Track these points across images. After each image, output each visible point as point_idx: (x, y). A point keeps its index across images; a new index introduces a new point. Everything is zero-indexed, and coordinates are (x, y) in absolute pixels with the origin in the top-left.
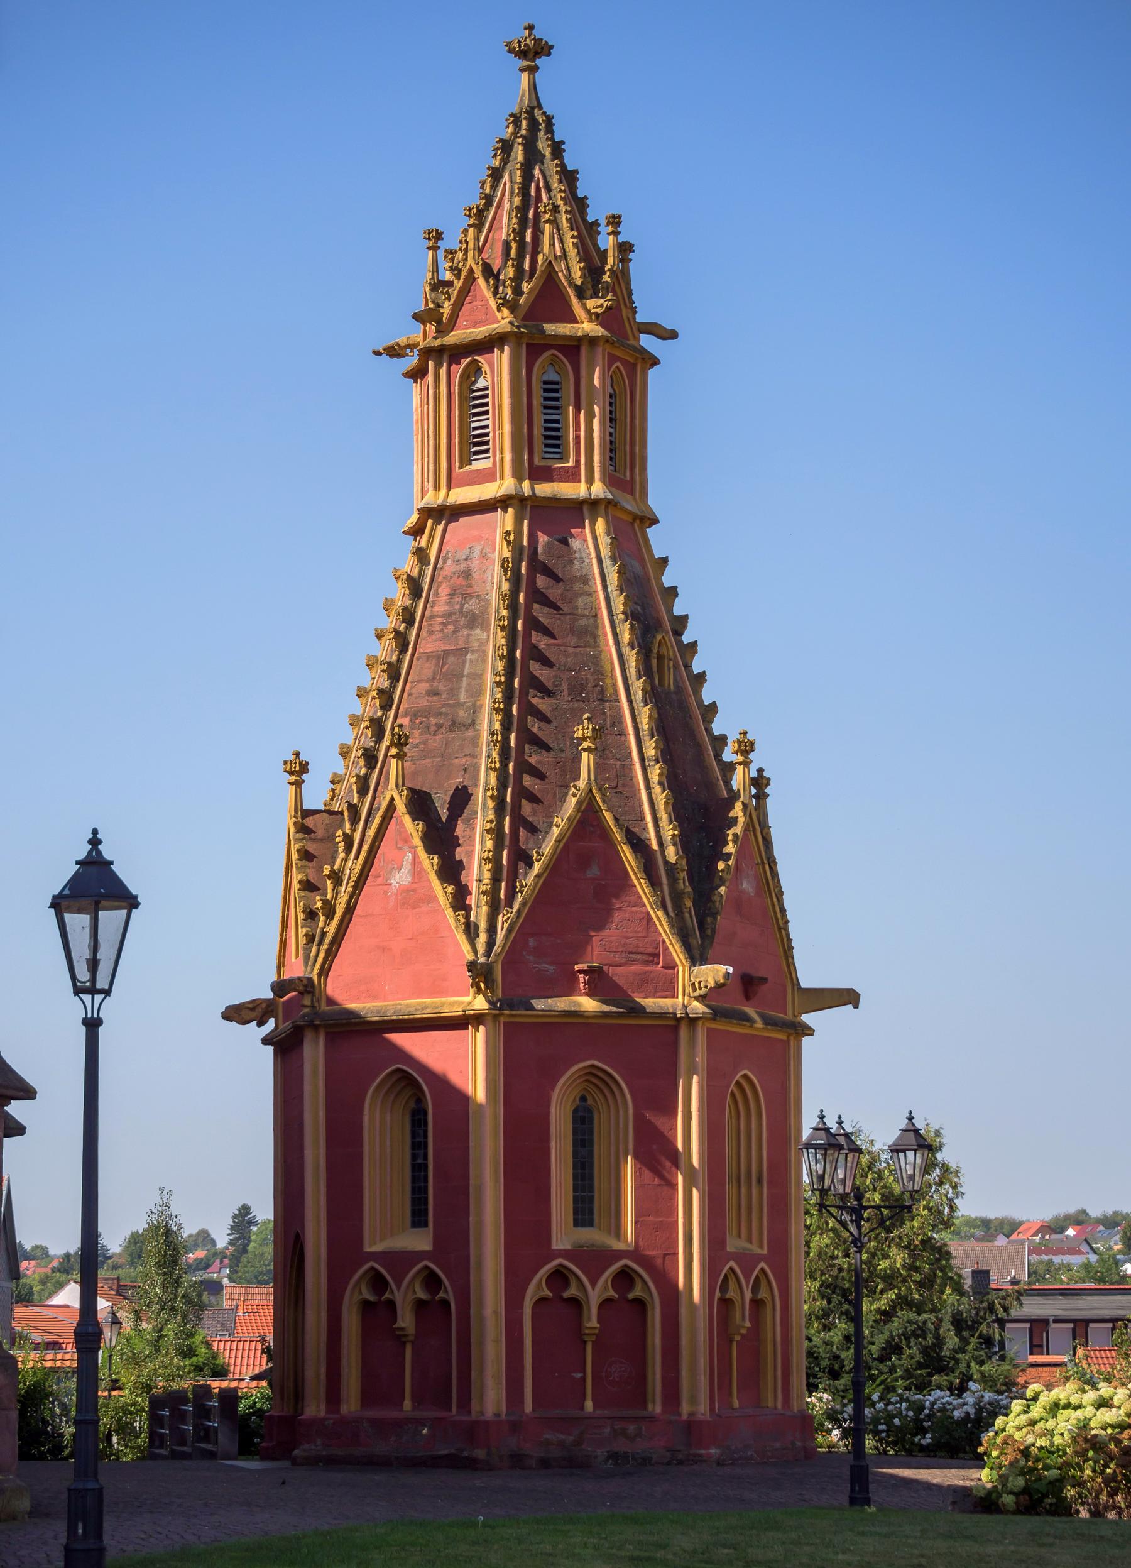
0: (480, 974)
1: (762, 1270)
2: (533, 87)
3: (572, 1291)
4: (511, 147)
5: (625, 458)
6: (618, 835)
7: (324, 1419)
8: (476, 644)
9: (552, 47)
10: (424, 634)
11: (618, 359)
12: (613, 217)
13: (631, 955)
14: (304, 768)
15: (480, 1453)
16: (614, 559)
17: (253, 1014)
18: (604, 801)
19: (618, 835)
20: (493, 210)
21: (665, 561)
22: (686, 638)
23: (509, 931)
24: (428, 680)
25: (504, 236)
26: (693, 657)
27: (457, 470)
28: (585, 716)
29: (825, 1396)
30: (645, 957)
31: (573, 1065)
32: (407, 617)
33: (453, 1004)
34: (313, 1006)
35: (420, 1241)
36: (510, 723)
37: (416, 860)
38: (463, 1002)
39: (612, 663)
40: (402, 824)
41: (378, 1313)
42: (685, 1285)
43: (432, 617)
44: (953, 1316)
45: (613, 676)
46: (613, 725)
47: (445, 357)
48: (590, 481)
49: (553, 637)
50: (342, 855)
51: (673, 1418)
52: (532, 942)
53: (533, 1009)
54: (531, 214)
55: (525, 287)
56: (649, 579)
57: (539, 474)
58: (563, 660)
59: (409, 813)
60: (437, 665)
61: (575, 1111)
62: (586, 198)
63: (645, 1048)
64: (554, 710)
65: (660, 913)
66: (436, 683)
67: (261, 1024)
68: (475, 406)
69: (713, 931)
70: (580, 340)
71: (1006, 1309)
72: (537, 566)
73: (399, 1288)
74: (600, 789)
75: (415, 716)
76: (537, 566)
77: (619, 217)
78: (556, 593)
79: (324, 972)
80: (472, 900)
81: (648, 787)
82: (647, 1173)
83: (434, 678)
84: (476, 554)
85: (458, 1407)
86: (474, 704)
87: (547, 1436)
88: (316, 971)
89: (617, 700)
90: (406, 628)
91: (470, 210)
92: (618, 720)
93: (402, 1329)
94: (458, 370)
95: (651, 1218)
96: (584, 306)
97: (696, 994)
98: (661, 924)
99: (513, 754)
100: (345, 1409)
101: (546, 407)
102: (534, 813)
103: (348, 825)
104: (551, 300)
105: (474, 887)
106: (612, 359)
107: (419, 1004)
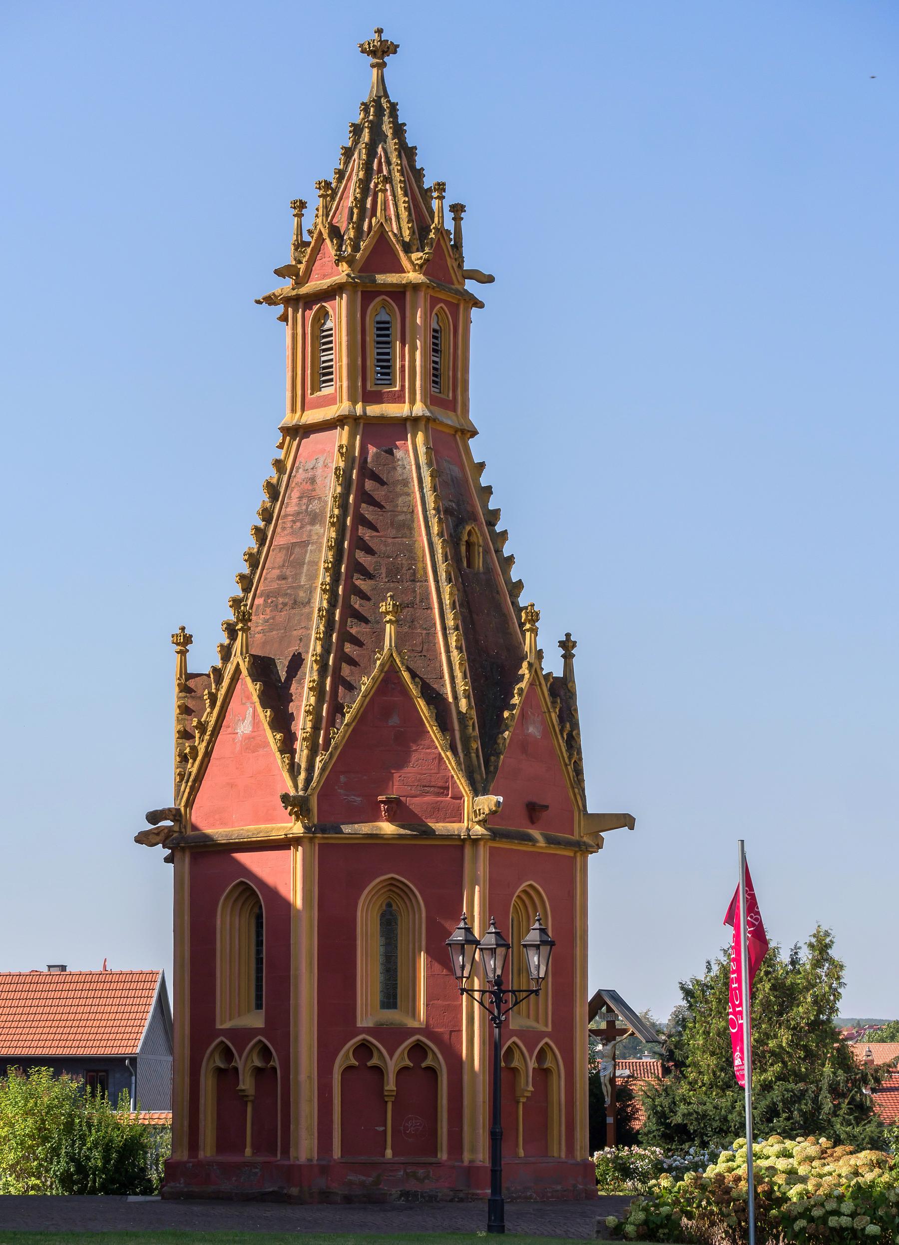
0: (298, 806)
2: (382, 80)
3: (374, 1061)
4: (362, 130)
5: (447, 380)
6: (414, 691)
7: (185, 1163)
8: (315, 537)
9: (398, 46)
10: (279, 530)
11: (441, 301)
12: (439, 184)
13: (425, 788)
14: (188, 640)
15: (294, 1191)
16: (429, 464)
17: (158, 839)
18: (403, 663)
19: (414, 691)
20: (344, 182)
21: (482, 465)
22: (498, 528)
23: (323, 769)
24: (279, 567)
25: (350, 204)
26: (504, 543)
27: (309, 396)
28: (389, 595)
29: (658, 1149)
30: (436, 790)
31: (375, 878)
32: (267, 516)
33: (279, 829)
34: (180, 832)
36: (336, 601)
38: (286, 827)
39: (424, 551)
40: (245, 684)
41: (227, 1076)
42: (467, 1056)
43: (286, 516)
44: (830, 1086)
45: (424, 561)
46: (421, 601)
47: (301, 304)
48: (413, 402)
49: (377, 531)
50: (208, 710)
51: (457, 1164)
52: (343, 778)
55: (363, 245)
56: (467, 481)
57: (371, 397)
59: (250, 675)
60: (286, 555)
61: (383, 915)
62: (422, 169)
63: (436, 864)
64: (373, 589)
68: (324, 344)
69: (496, 768)
70: (405, 286)
73: (240, 1057)
75: (268, 597)
76: (367, 473)
77: (444, 184)
78: (379, 494)
79: (189, 804)
80: (297, 745)
82: (437, 966)
83: (283, 566)
84: (320, 464)
86: (311, 587)
88: (183, 804)
89: (427, 581)
90: (266, 525)
91: (320, 183)
92: (426, 597)
93: (243, 1091)
94: (310, 314)
95: (440, 1002)
96: (410, 259)
97: (477, 819)
99: (337, 626)
100: (201, 1155)
101: (378, 343)
102: (352, 673)
103: (213, 686)
104: (382, 255)
105: (300, 735)
106: (434, 301)
107: (256, 829)
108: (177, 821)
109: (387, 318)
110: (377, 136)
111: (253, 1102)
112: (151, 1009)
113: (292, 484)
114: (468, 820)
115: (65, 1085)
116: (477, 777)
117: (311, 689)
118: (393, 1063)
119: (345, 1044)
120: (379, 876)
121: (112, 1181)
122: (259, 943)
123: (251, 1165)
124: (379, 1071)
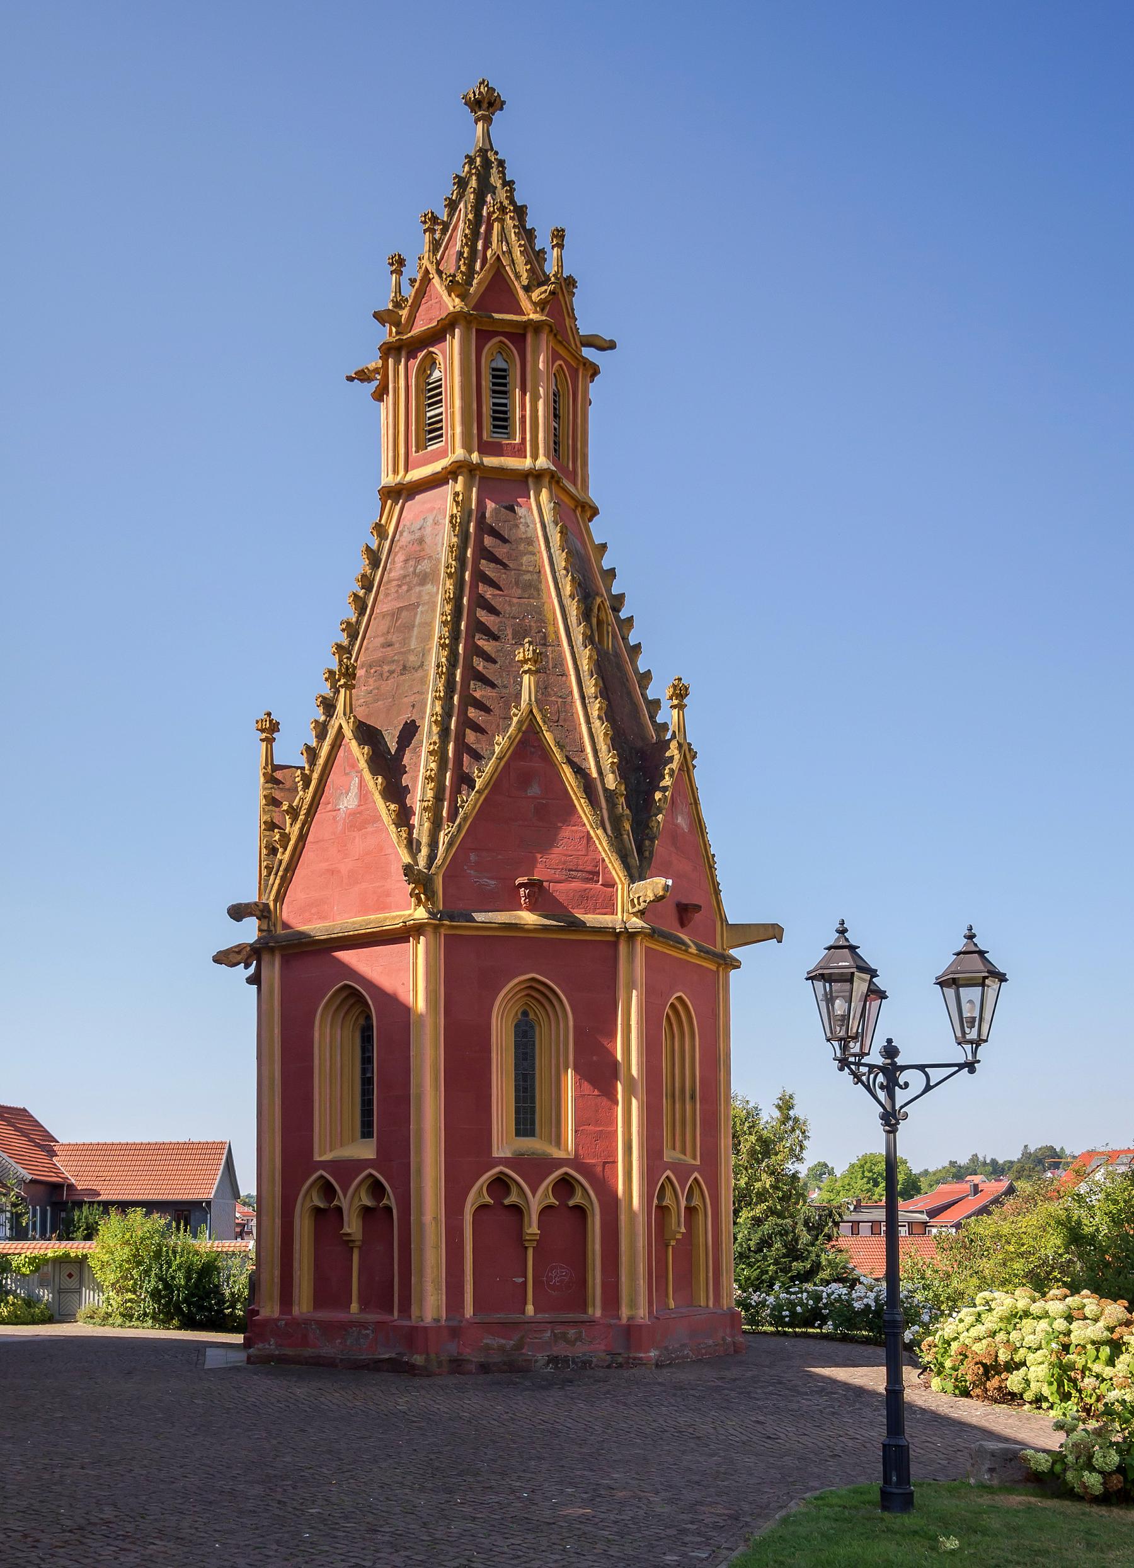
0: (421, 882)
1: (695, 1179)
2: (487, 135)
3: (513, 1198)
5: (568, 440)
6: (559, 756)
7: (278, 1320)
8: (426, 598)
9: (504, 103)
10: (381, 596)
14: (274, 727)
15: (418, 1359)
17: (239, 957)
21: (604, 546)
22: (623, 615)
23: (450, 844)
24: (383, 635)
26: (629, 630)
32: (367, 584)
35: (366, 1151)
36: (456, 661)
37: (362, 784)
39: (554, 613)
41: (327, 1218)
45: (555, 624)
46: (555, 667)
47: (404, 353)
48: (535, 457)
52: (473, 857)
53: (474, 921)
54: (482, 230)
57: (486, 448)
58: (508, 608)
63: (584, 961)
65: (600, 832)
66: (390, 636)
67: (247, 967)
69: (651, 853)
71: (840, 1215)
72: (484, 528)
73: (345, 1196)
74: (540, 710)
75: (371, 667)
76: (484, 528)
77: (563, 230)
78: (501, 551)
79: (280, 897)
80: (415, 820)
81: (588, 722)
85: (400, 1311)
87: (488, 1341)
88: (272, 898)
92: (560, 662)
93: (349, 1235)
94: (414, 364)
95: (591, 1127)
96: (530, 298)
97: (635, 910)
98: (601, 843)
99: (458, 687)
100: (296, 1311)
102: (478, 741)
108: (265, 917)
109: (503, 365)
110: (484, 188)
111: (360, 1248)
112: (222, 1167)
113: (396, 549)
114: (623, 912)
115: (155, 1221)
116: (631, 861)
117: (431, 753)
118: (537, 1200)
119: (477, 1179)
120: (517, 976)
121: (192, 1295)
122: (367, 1060)
124: (517, 1211)
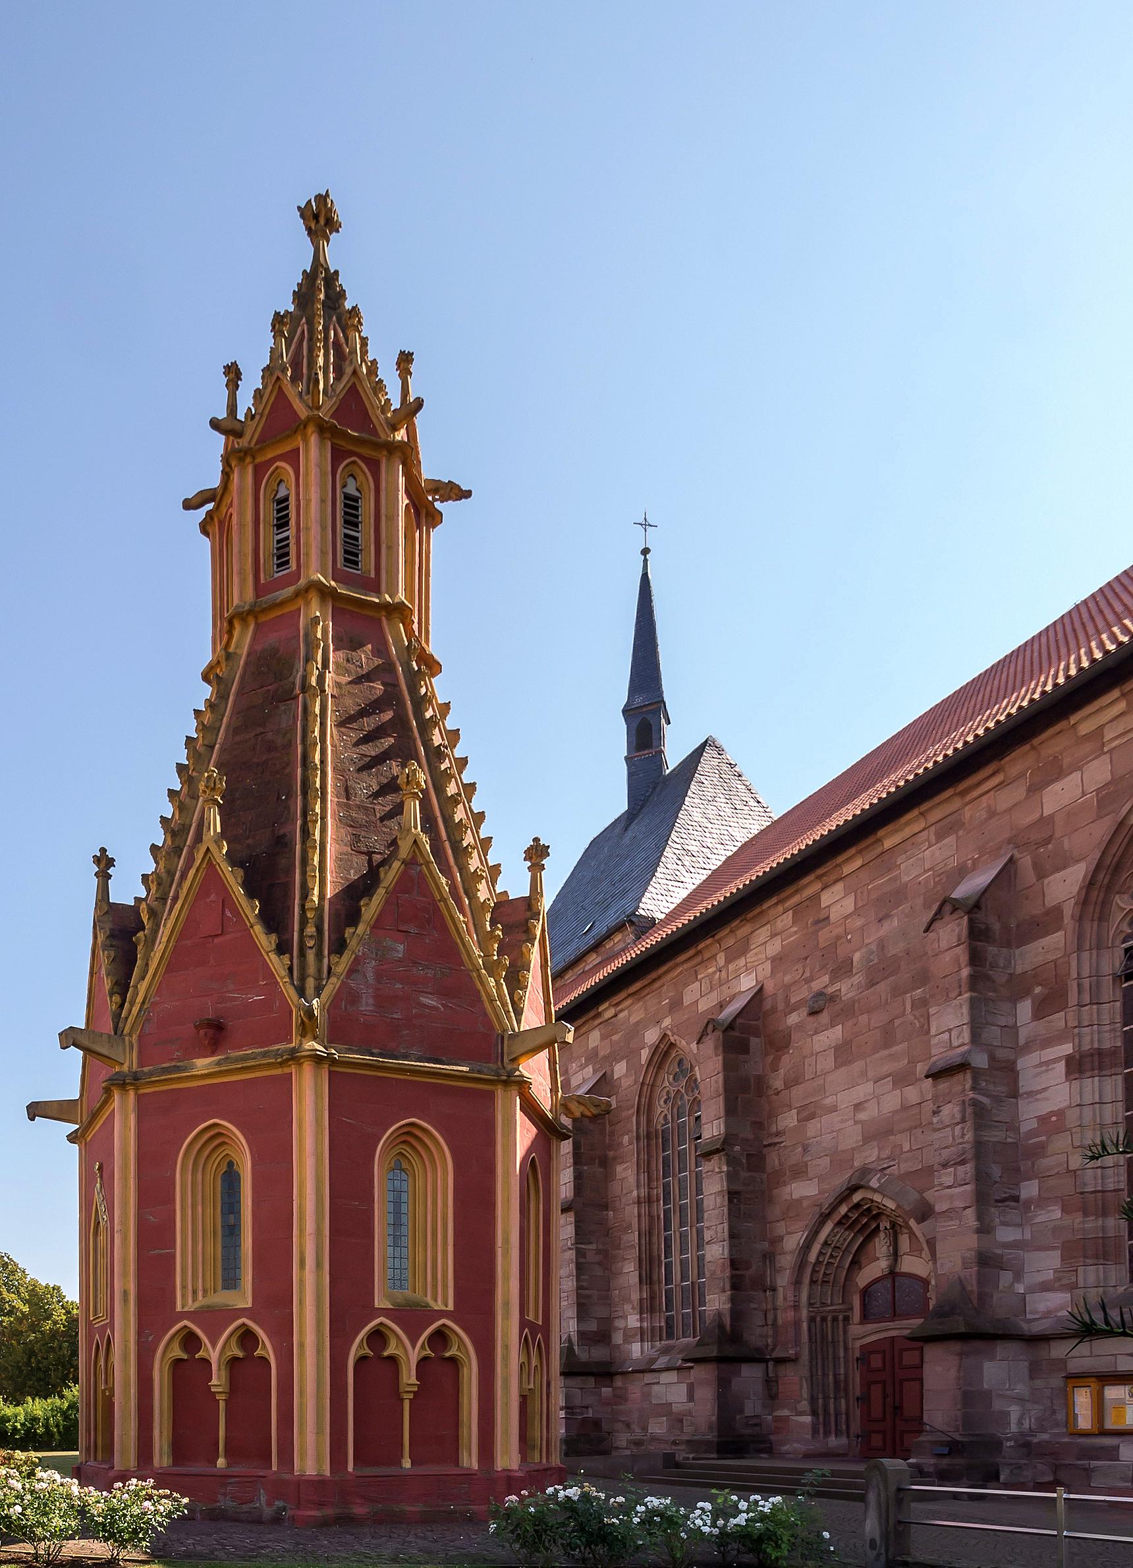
14: (111, 862)
123: (224, 1477)
